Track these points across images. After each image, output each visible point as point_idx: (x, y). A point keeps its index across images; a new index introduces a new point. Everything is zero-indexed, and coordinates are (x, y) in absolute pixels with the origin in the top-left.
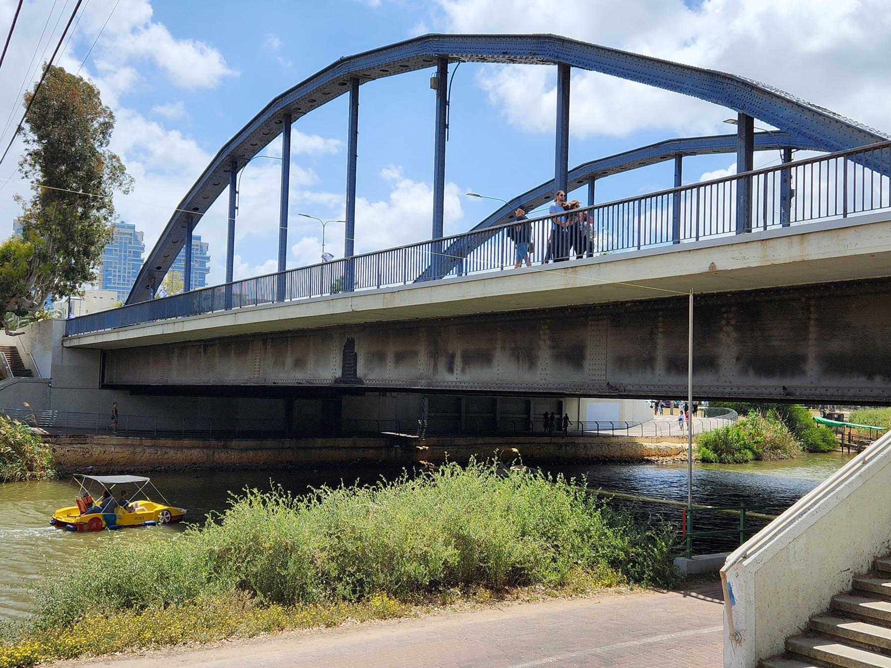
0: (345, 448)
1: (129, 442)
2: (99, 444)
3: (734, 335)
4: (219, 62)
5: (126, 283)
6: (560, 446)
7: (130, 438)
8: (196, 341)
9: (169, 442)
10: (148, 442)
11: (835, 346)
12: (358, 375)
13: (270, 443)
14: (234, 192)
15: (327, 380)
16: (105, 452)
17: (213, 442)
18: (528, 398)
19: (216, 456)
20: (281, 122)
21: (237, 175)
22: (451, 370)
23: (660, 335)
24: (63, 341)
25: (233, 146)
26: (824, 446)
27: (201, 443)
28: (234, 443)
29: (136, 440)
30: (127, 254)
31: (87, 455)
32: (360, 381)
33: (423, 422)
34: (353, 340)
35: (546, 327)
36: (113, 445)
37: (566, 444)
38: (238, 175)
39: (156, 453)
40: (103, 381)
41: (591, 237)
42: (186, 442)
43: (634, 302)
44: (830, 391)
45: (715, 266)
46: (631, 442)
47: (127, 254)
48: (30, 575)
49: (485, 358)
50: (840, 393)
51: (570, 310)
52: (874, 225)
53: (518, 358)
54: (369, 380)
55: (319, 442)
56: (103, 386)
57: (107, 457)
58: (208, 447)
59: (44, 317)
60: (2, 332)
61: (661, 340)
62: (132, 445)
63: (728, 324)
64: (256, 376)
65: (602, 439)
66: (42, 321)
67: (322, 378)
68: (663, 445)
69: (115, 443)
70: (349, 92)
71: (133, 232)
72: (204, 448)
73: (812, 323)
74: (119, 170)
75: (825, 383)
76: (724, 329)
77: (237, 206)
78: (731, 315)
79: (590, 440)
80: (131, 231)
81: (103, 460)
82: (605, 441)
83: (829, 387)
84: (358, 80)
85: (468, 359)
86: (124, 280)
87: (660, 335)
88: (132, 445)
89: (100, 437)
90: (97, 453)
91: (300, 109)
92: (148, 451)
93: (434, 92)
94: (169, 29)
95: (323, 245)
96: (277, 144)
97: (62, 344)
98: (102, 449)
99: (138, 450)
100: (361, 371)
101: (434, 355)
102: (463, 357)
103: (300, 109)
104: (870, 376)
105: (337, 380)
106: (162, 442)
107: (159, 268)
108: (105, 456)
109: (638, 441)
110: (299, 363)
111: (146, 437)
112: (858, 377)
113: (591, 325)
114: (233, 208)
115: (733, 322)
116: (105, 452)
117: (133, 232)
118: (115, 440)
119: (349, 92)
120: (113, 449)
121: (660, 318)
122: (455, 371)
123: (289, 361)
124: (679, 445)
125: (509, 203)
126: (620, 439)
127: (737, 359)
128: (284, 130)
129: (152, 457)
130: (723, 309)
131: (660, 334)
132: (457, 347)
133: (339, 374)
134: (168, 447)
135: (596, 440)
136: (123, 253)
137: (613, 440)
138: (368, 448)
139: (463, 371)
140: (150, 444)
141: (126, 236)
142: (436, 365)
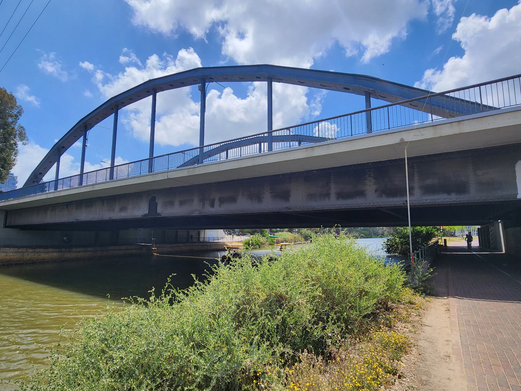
0: (123, 250)
1: (20, 251)
2: (3, 252)
3: (373, 181)
6: (202, 246)
8: (62, 203)
9: (42, 250)
11: (429, 182)
12: (158, 212)
13: (90, 249)
14: (85, 140)
15: (139, 215)
17: (64, 250)
18: (188, 230)
19: (65, 255)
20: (113, 109)
22: (212, 206)
23: (332, 184)
25: (59, 144)
26: (273, 244)
27: (57, 250)
28: (74, 250)
32: (159, 214)
33: (154, 239)
34: (155, 197)
35: (268, 184)
36: (11, 252)
37: (204, 245)
38: (88, 132)
42: (50, 250)
43: (317, 170)
44: (428, 201)
45: (404, 140)
46: (224, 244)
48: (4, 373)
49: (233, 200)
50: (433, 201)
51: (281, 176)
52: (505, 114)
53: (252, 199)
54: (165, 214)
55: (112, 248)
56: (6, 226)
57: (8, 258)
58: (61, 252)
61: (333, 186)
62: (22, 252)
63: (370, 177)
64: (97, 216)
65: (215, 243)
67: (136, 214)
68: (233, 244)
69: (12, 251)
70: (152, 96)
72: (59, 252)
73: (416, 173)
75: (425, 198)
76: (368, 179)
78: (371, 173)
79: (212, 244)
81: (6, 260)
82: (217, 243)
83: (427, 199)
84: (156, 90)
85: (222, 201)
87: (332, 184)
88: (22, 252)
91: (123, 103)
92: (30, 254)
96: (78, 144)
98: (5, 254)
99: (25, 254)
100: (159, 210)
101: (203, 200)
103: (123, 103)
104: (449, 193)
106: (38, 250)
107: (41, 173)
108: (7, 257)
109: (226, 243)
111: (30, 248)
112: (443, 194)
113: (293, 182)
114: (84, 146)
115: (372, 175)
116: (6, 255)
118: (12, 250)
119: (152, 96)
121: (332, 177)
122: (215, 207)
123: (117, 209)
124: (238, 244)
126: (220, 243)
127: (376, 191)
128: (115, 112)
130: (367, 170)
132: (216, 196)
133: (146, 212)
135: (208, 244)
137: (219, 243)
138: (133, 249)
139: (220, 206)
140: (31, 251)
142: (204, 204)
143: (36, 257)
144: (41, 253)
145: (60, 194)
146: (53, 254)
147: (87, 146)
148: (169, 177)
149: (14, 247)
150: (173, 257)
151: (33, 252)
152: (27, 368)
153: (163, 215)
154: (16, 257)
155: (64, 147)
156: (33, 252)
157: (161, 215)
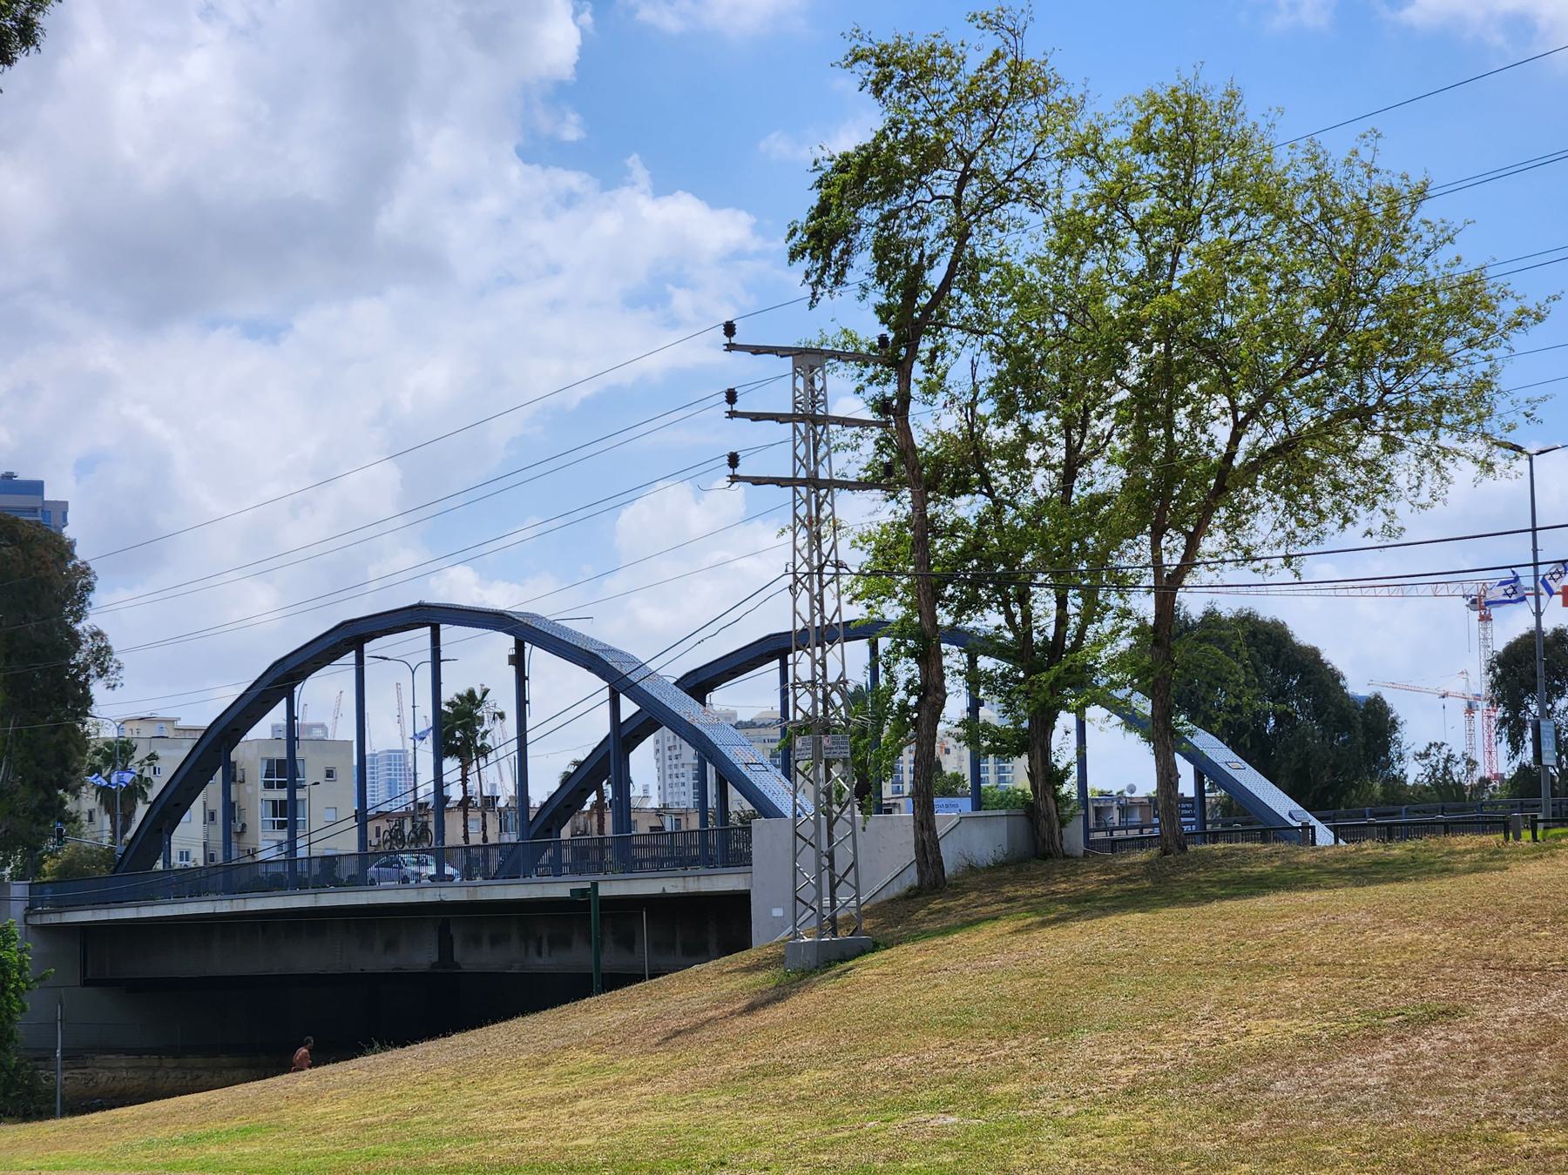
1: (144, 1063)
7: (145, 1056)
10: (169, 1062)
16: (114, 1078)
21: (296, 689)
22: (539, 954)
24: (26, 916)
29: (154, 1060)
31: (91, 1084)
38: (297, 689)
39: (185, 1078)
40: (85, 975)
49: (566, 943)
56: (86, 983)
69: (124, 1064)
74: (102, 655)
89: (103, 1057)
90: (104, 1079)
92: (172, 1075)
93: (513, 668)
95: (414, 707)
97: (25, 921)
98: (109, 1074)
99: (159, 1073)
100: (457, 955)
102: (549, 941)
105: (433, 965)
107: (177, 805)
110: (390, 945)
116: (114, 1078)
118: (123, 1061)
120: (125, 1073)
125: (682, 678)
129: (178, 1084)
133: (435, 958)
134: (200, 1069)
143: (190, 1083)
144: (200, 1073)
145: (245, 906)
146: (235, 1073)
147: (297, 739)
148: (444, 898)
149: (128, 1052)
150: (119, 902)
151: (176, 1068)
152: (412, 770)
153: (466, 968)
154: (136, 1082)
155: (237, 730)
156: (176, 1068)
157: (460, 968)
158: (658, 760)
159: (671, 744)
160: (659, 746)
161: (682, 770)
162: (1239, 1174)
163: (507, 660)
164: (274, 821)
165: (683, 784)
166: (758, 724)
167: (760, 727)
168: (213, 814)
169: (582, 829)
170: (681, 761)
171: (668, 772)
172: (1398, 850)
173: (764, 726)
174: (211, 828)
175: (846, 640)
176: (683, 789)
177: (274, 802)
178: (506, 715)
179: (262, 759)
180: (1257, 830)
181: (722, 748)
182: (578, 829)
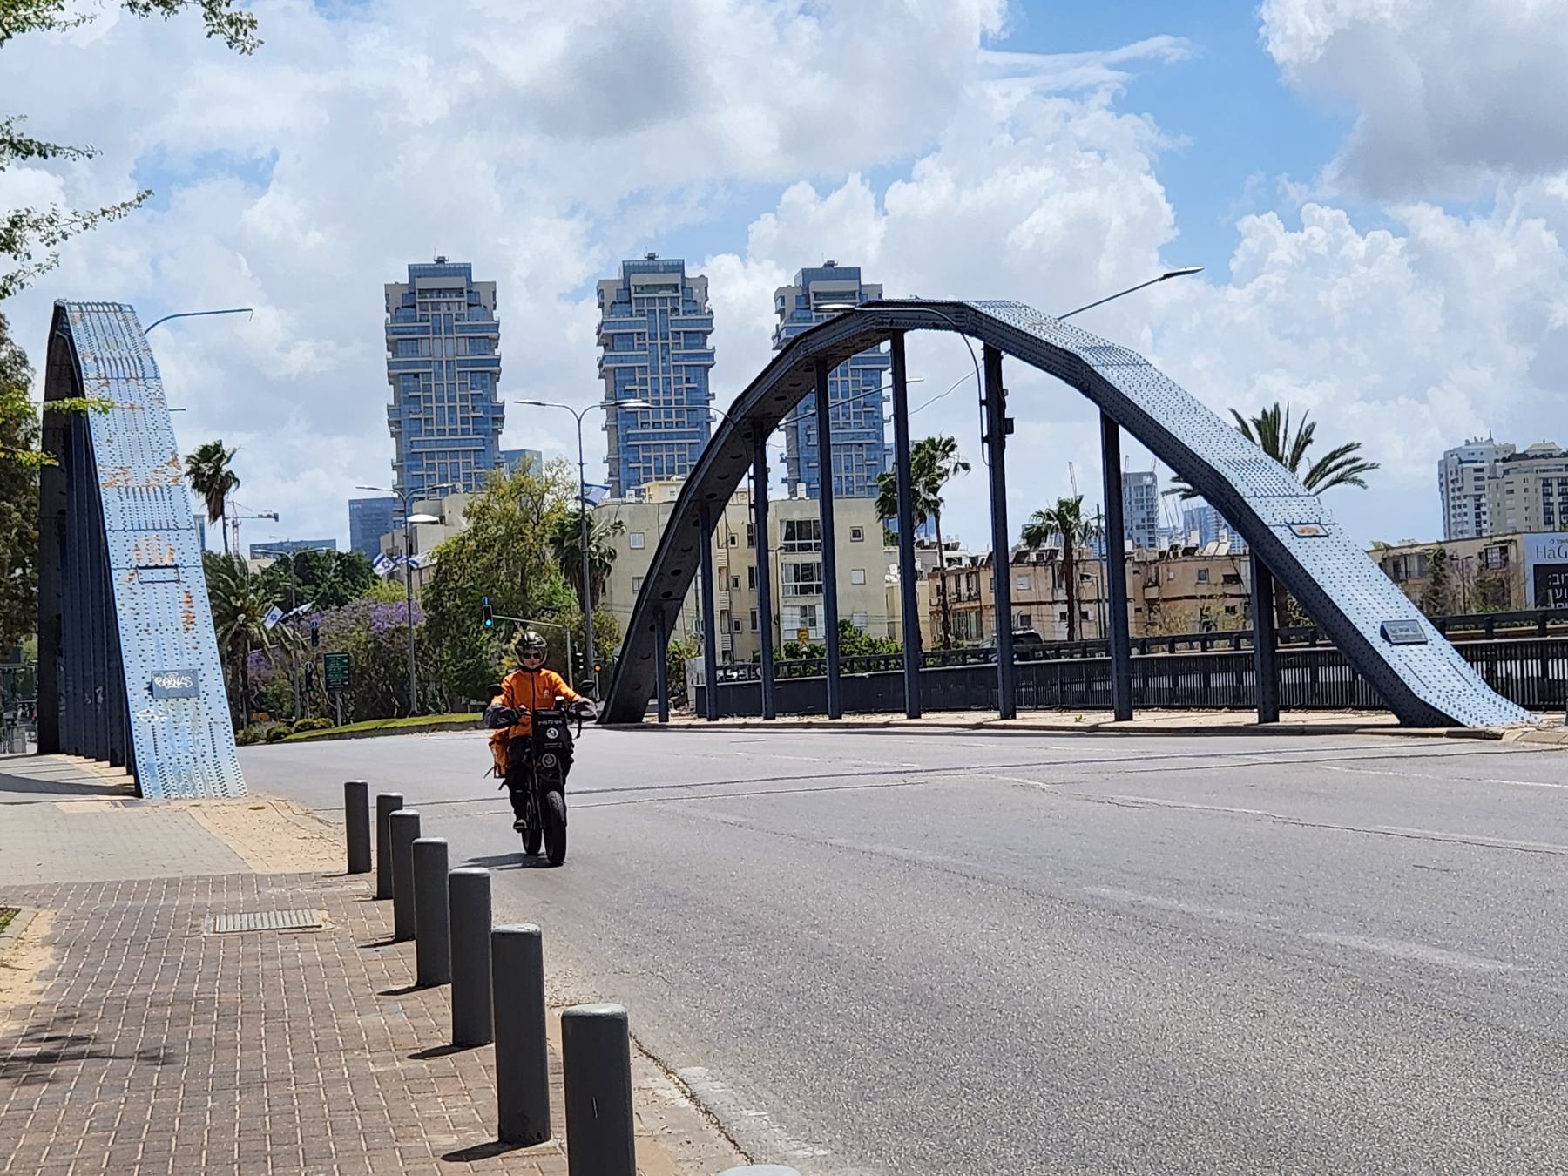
4: (330, 18)
5: (674, 419)
30: (670, 341)
41: (1293, 637)
47: (670, 341)
59: (247, 609)
60: (5, 255)
66: (166, 1014)
71: (679, 281)
77: (984, 408)
80: (674, 279)
86: (669, 415)
94: (48, 171)
117: (679, 281)
131: (687, 275)
136: (659, 342)
141: (663, 293)
158: (1442, 493)
159: (1454, 477)
160: (1443, 480)
161: (1465, 501)
162: (1566, 869)
163: (204, 444)
164: (796, 586)
165: (1466, 514)
166: (1530, 455)
167: (1533, 458)
168: (737, 580)
169: (1154, 579)
170: (1464, 493)
171: (1452, 503)
172: (806, 720)
173: (1535, 457)
174: (735, 595)
175: (726, 417)
176: (1466, 519)
177: (796, 566)
178: (971, 466)
179: (781, 522)
180: (930, 666)
181: (1253, 503)
182: (1150, 580)
